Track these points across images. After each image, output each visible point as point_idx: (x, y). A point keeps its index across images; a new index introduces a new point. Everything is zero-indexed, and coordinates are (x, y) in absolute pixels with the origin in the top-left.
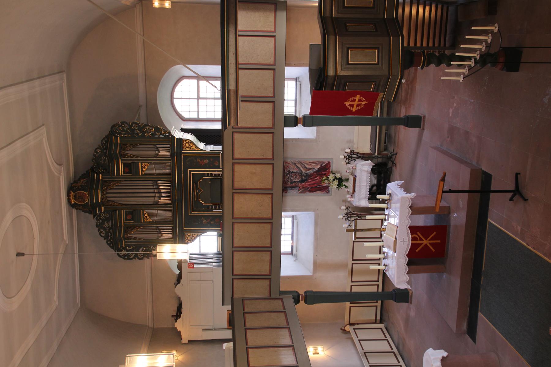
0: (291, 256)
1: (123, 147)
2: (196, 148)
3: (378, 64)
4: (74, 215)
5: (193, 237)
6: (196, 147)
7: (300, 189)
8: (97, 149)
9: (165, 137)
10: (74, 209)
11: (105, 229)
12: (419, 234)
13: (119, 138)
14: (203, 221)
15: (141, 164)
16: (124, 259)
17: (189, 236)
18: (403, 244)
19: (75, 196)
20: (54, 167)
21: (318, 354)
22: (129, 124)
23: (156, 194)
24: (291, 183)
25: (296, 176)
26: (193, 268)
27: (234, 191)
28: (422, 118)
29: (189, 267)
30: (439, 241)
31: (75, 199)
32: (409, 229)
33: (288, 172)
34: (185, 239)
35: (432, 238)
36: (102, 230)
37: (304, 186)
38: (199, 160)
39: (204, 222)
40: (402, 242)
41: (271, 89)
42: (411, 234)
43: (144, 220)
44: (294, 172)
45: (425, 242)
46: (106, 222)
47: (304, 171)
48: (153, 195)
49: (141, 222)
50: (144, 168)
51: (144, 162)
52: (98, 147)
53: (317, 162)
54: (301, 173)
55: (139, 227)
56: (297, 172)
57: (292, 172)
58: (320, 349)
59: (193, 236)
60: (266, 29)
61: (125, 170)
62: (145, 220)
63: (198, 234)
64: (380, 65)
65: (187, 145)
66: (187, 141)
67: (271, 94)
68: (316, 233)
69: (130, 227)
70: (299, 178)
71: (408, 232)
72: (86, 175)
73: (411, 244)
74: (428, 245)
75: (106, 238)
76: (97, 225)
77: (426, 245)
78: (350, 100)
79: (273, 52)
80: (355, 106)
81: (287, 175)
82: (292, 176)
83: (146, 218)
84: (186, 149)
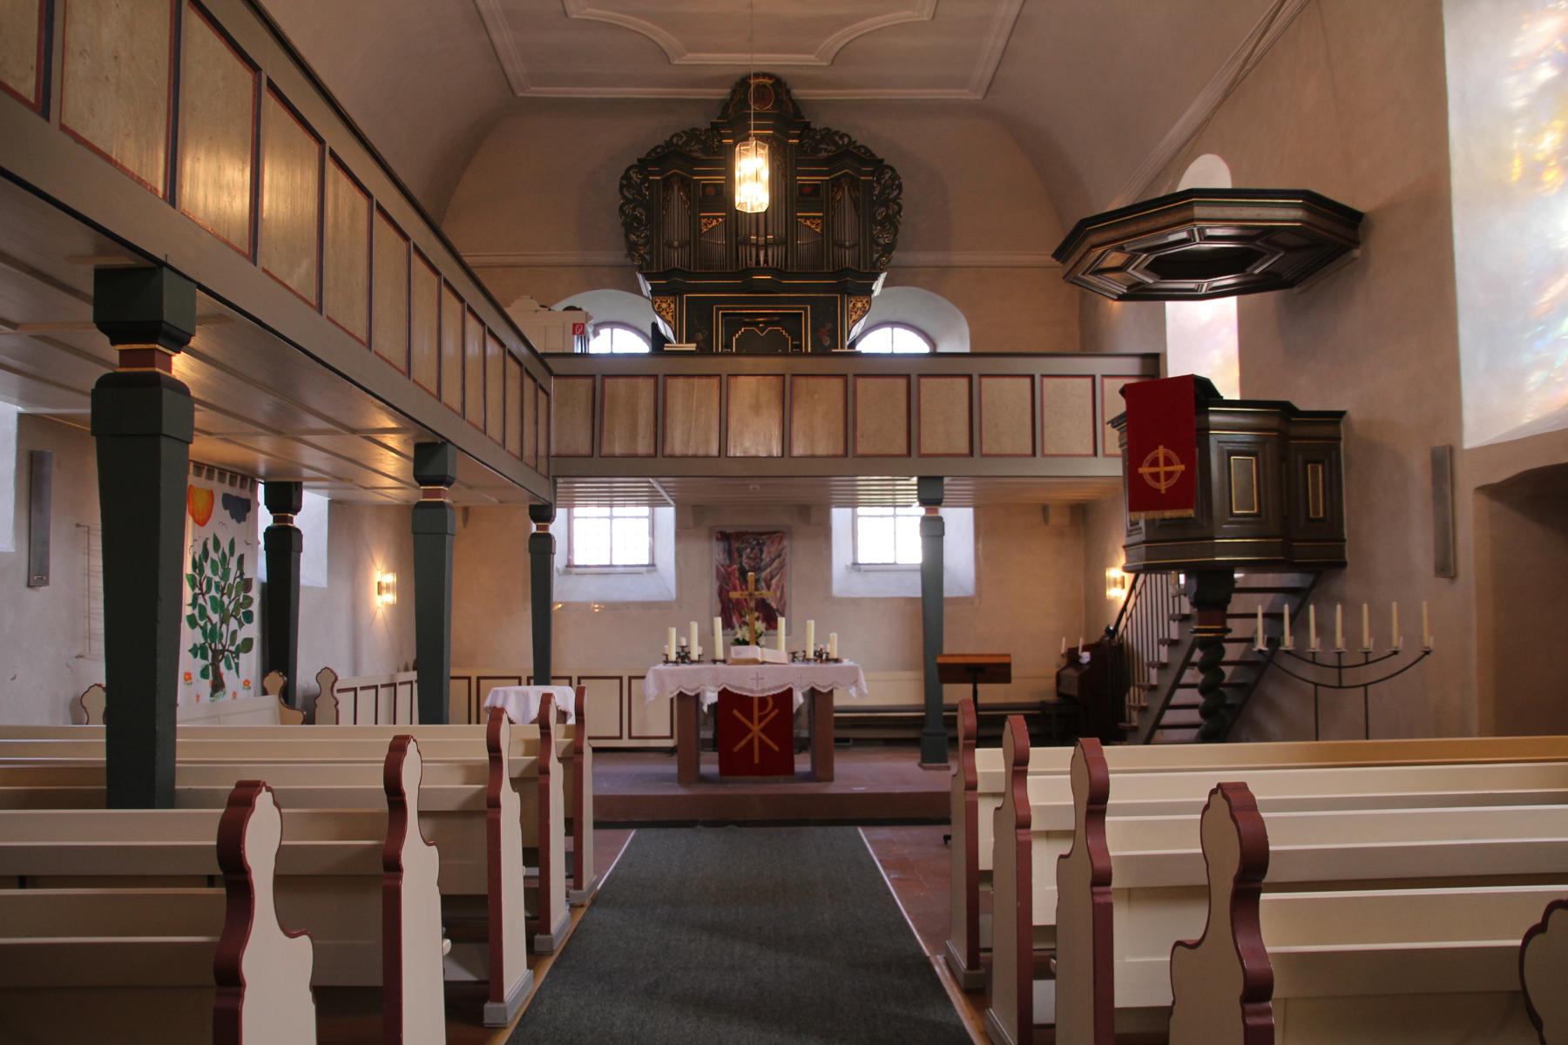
0: (566, 563)
1: (854, 184)
3: (1232, 515)
4: (709, 91)
5: (668, 313)
6: (855, 322)
7: (726, 567)
8: (849, 137)
9: (875, 264)
10: (729, 91)
11: (686, 143)
12: (773, 714)
13: (871, 178)
14: (700, 334)
15: (819, 218)
16: (623, 178)
17: (670, 305)
18: (752, 679)
19: (764, 86)
20: (834, 41)
21: (379, 593)
22: (897, 197)
23: (763, 239)
24: (738, 549)
25: (754, 559)
26: (574, 333)
27: (788, 378)
28: (947, 764)
29: (574, 325)
30: (757, 761)
31: (758, 87)
32: (785, 689)
33: (761, 541)
34: (661, 298)
35: (768, 746)
36: (685, 138)
37: (732, 576)
38: (829, 326)
40: (760, 676)
41: (996, 450)
42: (774, 696)
44: (761, 554)
45: (756, 728)
46: (701, 146)
47: (764, 574)
48: (762, 231)
49: (700, 212)
50: (811, 223)
51: (823, 222)
52: (853, 140)
53: (782, 602)
54: (759, 568)
55: (689, 208)
56: (762, 560)
57: (761, 551)
58: (390, 598)
60: (1107, 438)
64: (1231, 519)
65: (859, 305)
66: (866, 305)
67: (985, 450)
68: (627, 605)
69: (690, 191)
70: (749, 565)
71: (781, 687)
72: (798, 114)
73: (752, 698)
74: (749, 736)
75: (669, 143)
76: (695, 129)
77: (750, 731)
78: (1171, 453)
79: (1065, 452)
80: (1153, 470)
81: (755, 539)
82: (752, 549)
84: (656, 302)
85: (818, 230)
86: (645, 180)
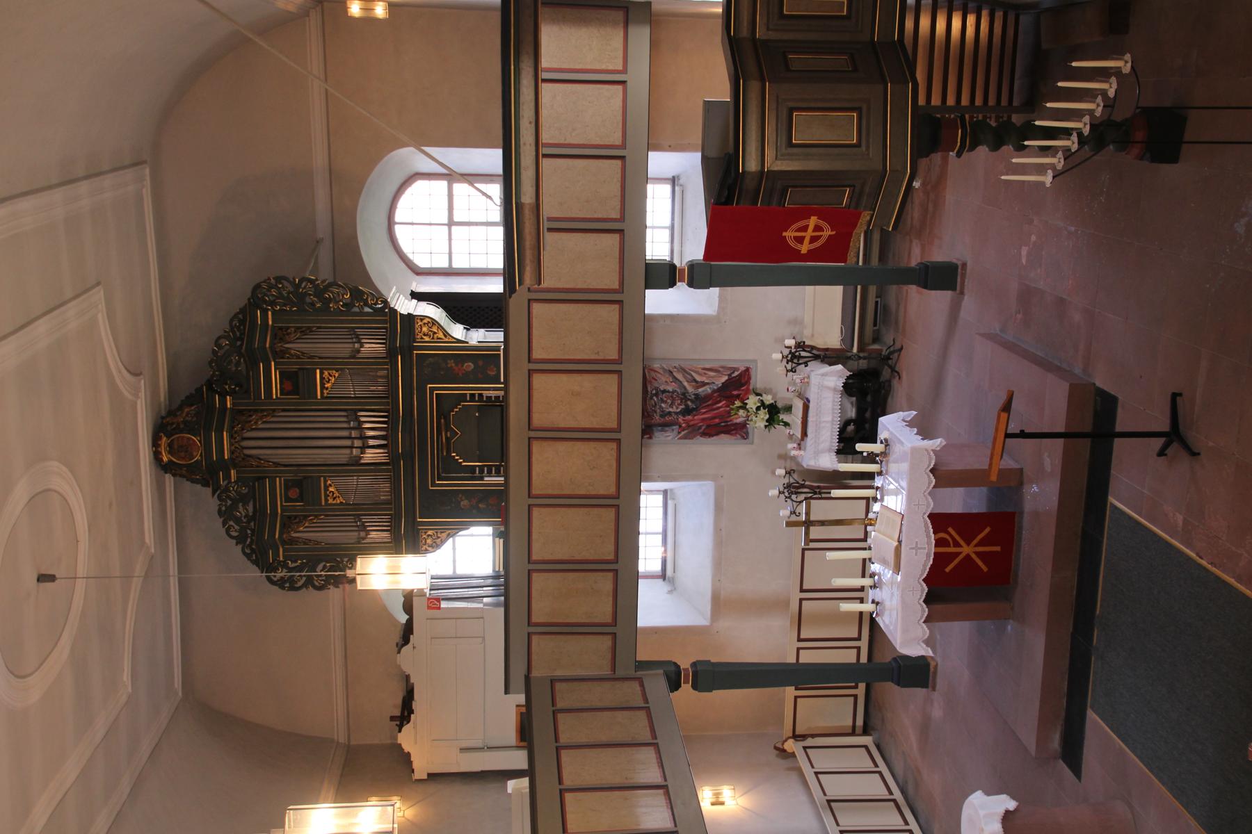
0: (660, 581)
1: (280, 334)
2: (445, 336)
3: (858, 145)
4: (168, 490)
5: (439, 537)
6: (446, 334)
7: (681, 429)
8: (219, 338)
9: (376, 310)
10: (168, 476)
11: (238, 520)
12: (953, 533)
13: (270, 313)
14: (462, 503)
15: (321, 373)
16: (283, 588)
17: (429, 535)
18: (916, 554)
19: (170, 445)
20: (122, 379)
21: (722, 803)
22: (292, 283)
23: (355, 441)
24: (661, 416)
25: (673, 400)
26: (439, 608)
27: (532, 434)
28: (960, 267)
29: (429, 608)
30: (998, 549)
31: (171, 451)
32: (929, 521)
33: (654, 392)
35: (982, 540)
36: (231, 523)
38: (451, 363)
39: (464, 505)
40: (914, 551)
41: (616, 203)
42: (935, 533)
43: (326, 500)
44: (668, 392)
45: (966, 550)
46: (241, 504)
47: (690, 389)
48: (348, 443)
49: (321, 505)
50: (328, 382)
51: (326, 369)
52: (222, 333)
53: (720, 369)
54: (684, 394)
55: (316, 516)
56: (674, 392)
57: (664, 391)
58: (727, 792)
59: (439, 535)
60: (604, 67)
61: (283, 386)
62: (331, 501)
63: (450, 531)
64: (864, 148)
65: (425, 329)
66: (425, 321)
67: (615, 214)
68: (718, 530)
69: (296, 517)
70: (680, 405)
71: (927, 527)
73: (935, 553)
74: (973, 556)
75: (240, 540)
76: (220, 511)
77: (968, 556)
78: (795, 226)
79: (620, 118)
80: (807, 240)
81: (651, 398)
82: (663, 401)
83: (331, 495)
85: (337, 375)
86: (285, 566)
